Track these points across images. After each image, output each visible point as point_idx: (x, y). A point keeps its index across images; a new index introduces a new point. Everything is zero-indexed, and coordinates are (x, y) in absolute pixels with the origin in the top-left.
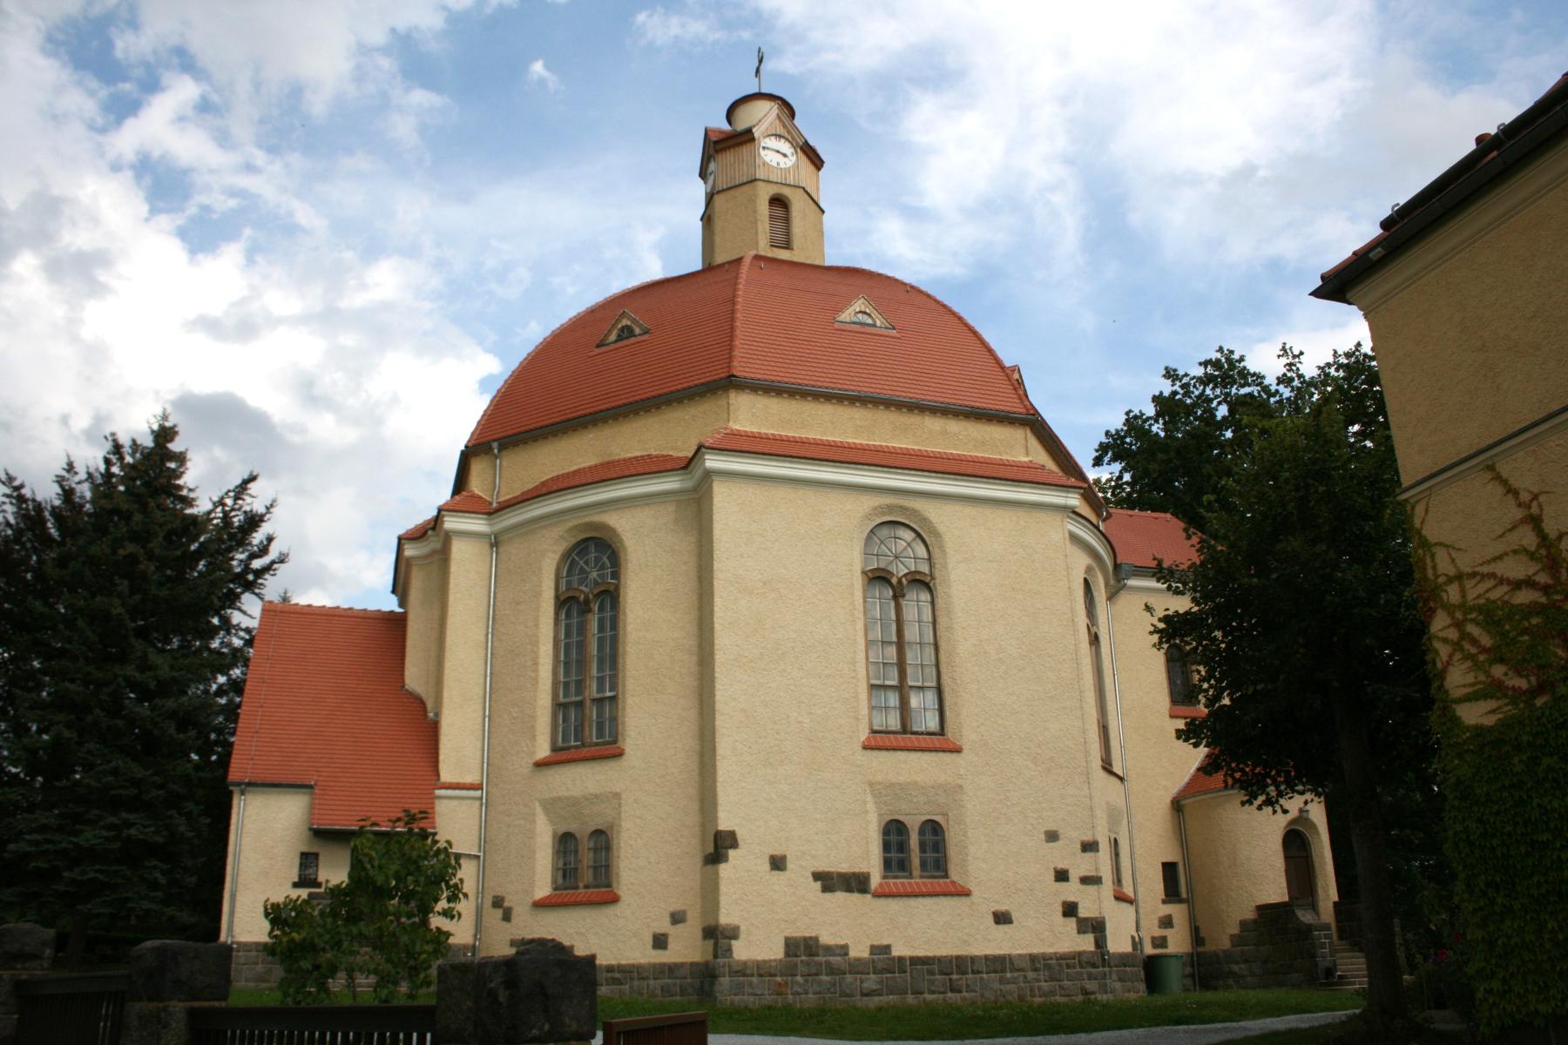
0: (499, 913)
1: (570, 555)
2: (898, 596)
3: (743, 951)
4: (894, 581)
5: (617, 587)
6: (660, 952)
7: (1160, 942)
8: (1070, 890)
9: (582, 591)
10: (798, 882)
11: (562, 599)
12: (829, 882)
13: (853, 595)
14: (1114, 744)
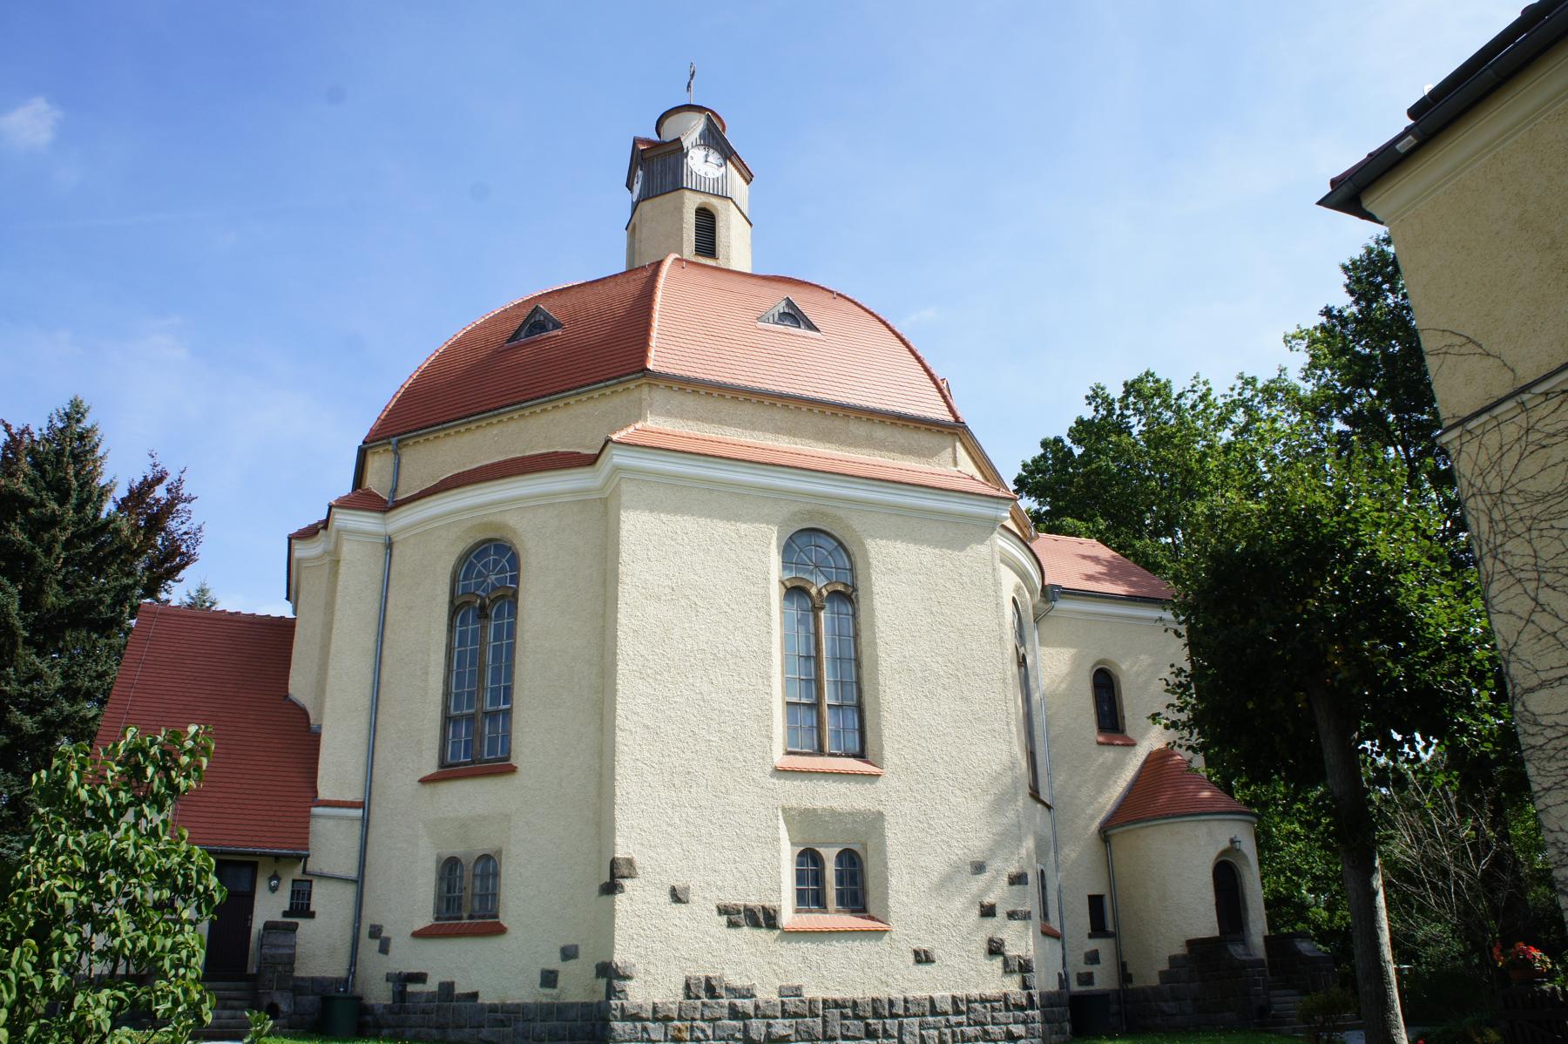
0: (376, 943)
1: (467, 558)
2: (816, 610)
3: (638, 994)
4: (814, 591)
5: (515, 593)
6: (548, 991)
7: (1087, 979)
8: (991, 927)
9: (478, 596)
10: (702, 920)
11: (457, 603)
13: (769, 604)
14: (1041, 770)
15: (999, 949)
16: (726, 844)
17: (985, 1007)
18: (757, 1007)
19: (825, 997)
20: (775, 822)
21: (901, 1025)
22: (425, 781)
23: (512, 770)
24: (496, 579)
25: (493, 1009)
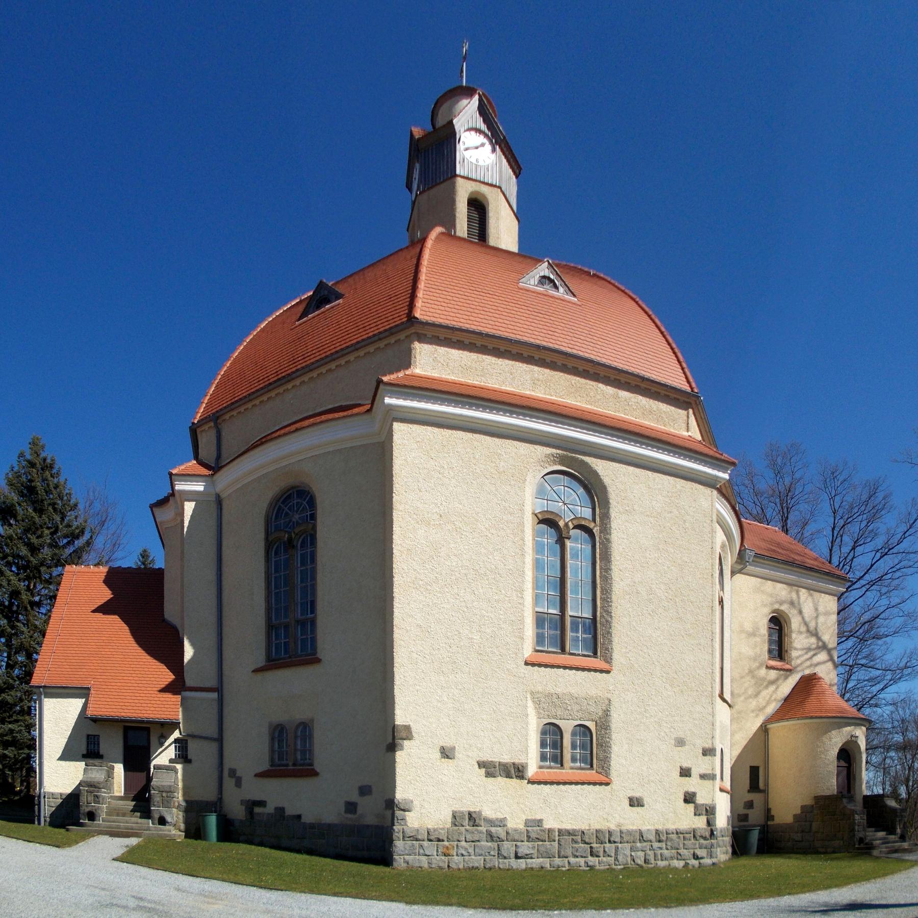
0: (233, 780)
4: (561, 524)
6: (350, 816)
9: (286, 532)
11: (270, 539)
12: (490, 769)
13: (523, 531)
15: (692, 799)
16: (484, 717)
17: (679, 837)
18: (507, 833)
19: (560, 827)
20: (524, 702)
21: (617, 848)
22: (256, 671)
23: (318, 661)
24: (299, 518)
25: (312, 826)
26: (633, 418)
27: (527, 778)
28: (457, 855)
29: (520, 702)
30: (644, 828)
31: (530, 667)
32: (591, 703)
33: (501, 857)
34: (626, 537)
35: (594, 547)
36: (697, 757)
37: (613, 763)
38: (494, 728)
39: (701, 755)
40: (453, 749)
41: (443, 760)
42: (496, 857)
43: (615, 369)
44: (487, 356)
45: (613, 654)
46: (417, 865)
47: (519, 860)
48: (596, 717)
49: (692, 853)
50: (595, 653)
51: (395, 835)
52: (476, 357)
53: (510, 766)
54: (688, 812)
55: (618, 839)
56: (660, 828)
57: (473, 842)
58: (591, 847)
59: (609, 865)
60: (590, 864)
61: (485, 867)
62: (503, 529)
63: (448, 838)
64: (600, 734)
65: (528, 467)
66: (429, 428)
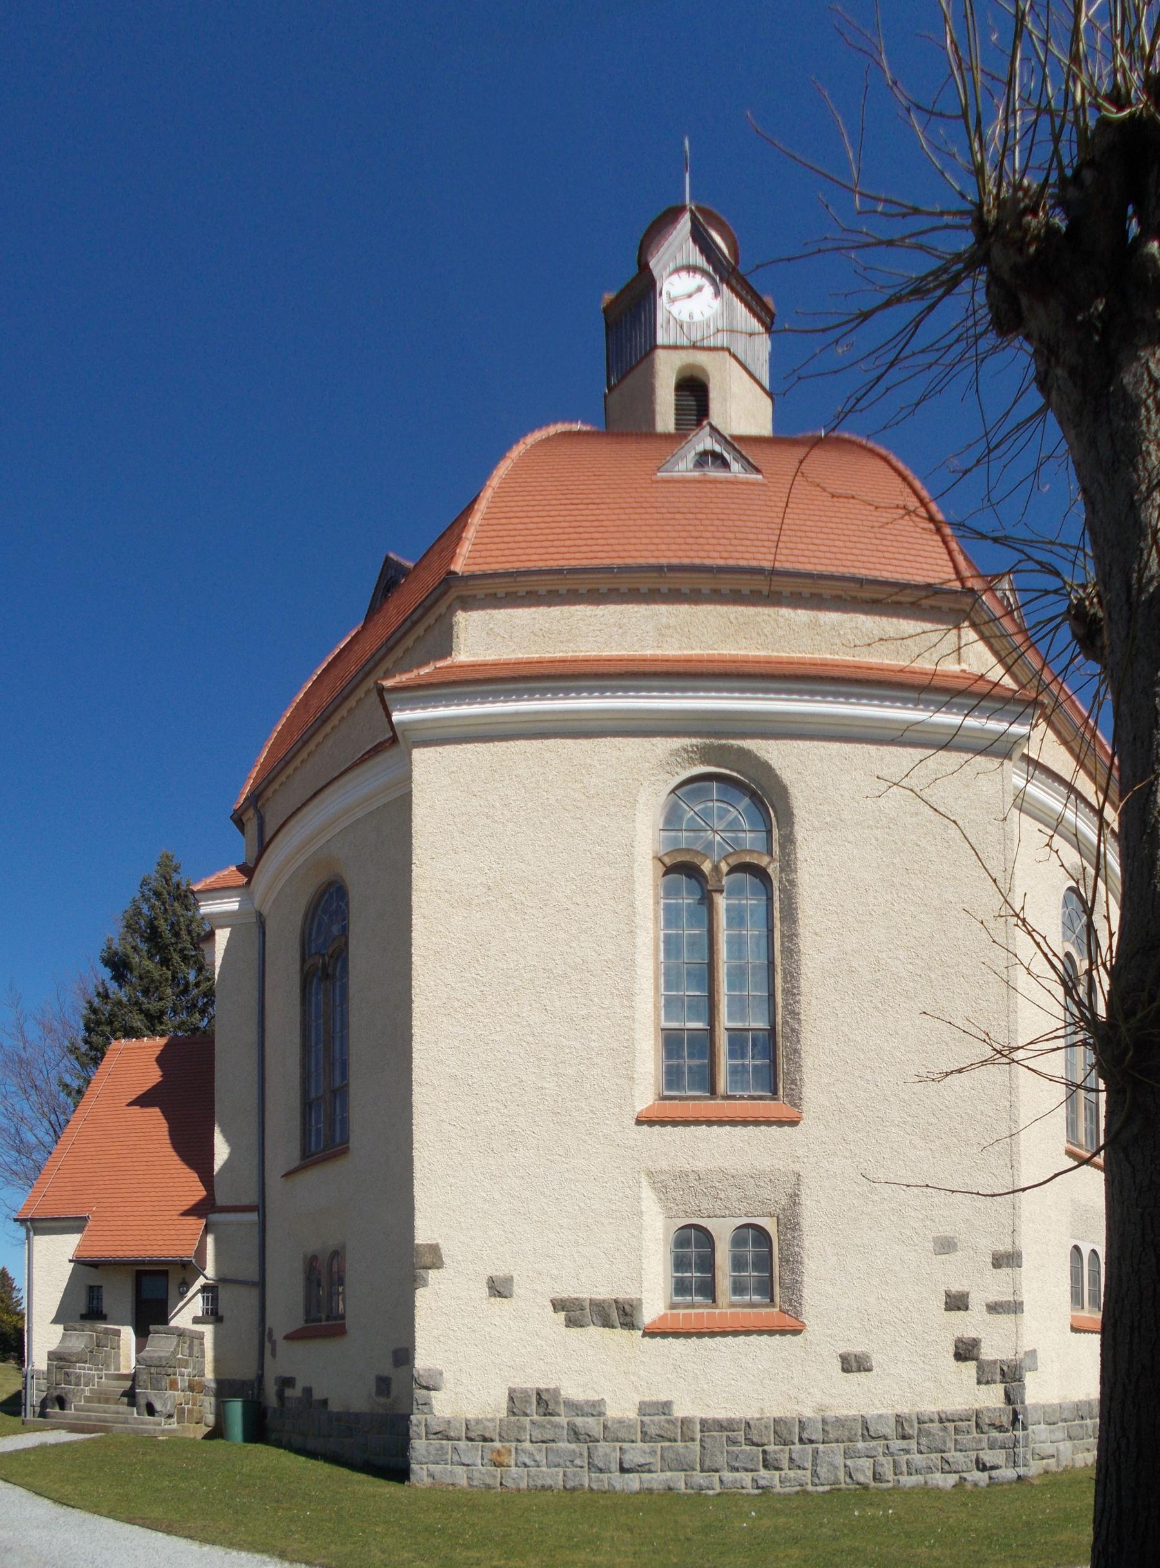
4: (706, 867)
18: (605, 1427)
19: (704, 1416)
21: (816, 1452)
25: (338, 1417)
26: (847, 658)
27: (643, 1327)
28: (516, 1465)
29: (628, 1192)
30: (871, 1412)
31: (645, 1128)
32: (762, 1184)
33: (593, 1469)
34: (825, 872)
35: (770, 899)
36: (981, 1272)
37: (806, 1293)
38: (581, 1241)
39: (990, 1266)
40: (509, 1280)
41: (493, 1299)
42: (586, 1469)
43: (810, 576)
44: (577, 607)
45: (804, 1090)
46: (449, 1481)
47: (626, 1475)
48: (776, 1209)
49: (974, 1458)
50: (775, 1091)
51: (413, 1430)
52: (558, 612)
53: (610, 1306)
54: (965, 1377)
55: (817, 1436)
56: (906, 1411)
57: (543, 1442)
58: (764, 1452)
59: (801, 1485)
60: (762, 1482)
61: (564, 1487)
62: (596, 892)
63: (500, 1435)
64: (785, 1240)
65: (641, 779)
66: (470, 746)
